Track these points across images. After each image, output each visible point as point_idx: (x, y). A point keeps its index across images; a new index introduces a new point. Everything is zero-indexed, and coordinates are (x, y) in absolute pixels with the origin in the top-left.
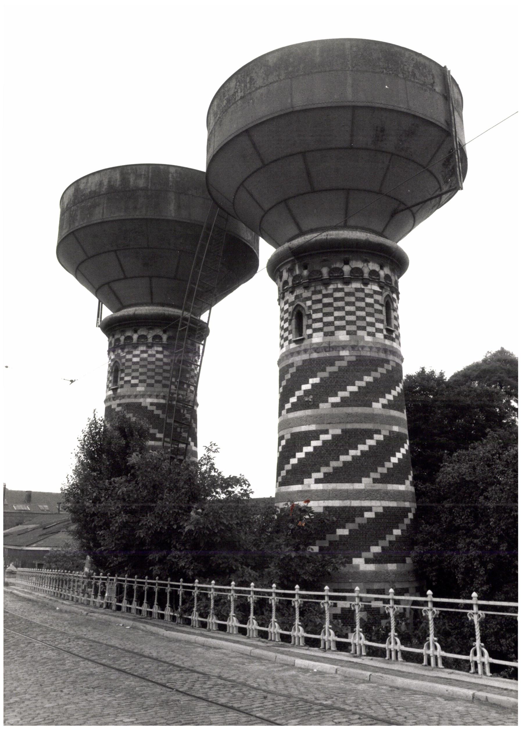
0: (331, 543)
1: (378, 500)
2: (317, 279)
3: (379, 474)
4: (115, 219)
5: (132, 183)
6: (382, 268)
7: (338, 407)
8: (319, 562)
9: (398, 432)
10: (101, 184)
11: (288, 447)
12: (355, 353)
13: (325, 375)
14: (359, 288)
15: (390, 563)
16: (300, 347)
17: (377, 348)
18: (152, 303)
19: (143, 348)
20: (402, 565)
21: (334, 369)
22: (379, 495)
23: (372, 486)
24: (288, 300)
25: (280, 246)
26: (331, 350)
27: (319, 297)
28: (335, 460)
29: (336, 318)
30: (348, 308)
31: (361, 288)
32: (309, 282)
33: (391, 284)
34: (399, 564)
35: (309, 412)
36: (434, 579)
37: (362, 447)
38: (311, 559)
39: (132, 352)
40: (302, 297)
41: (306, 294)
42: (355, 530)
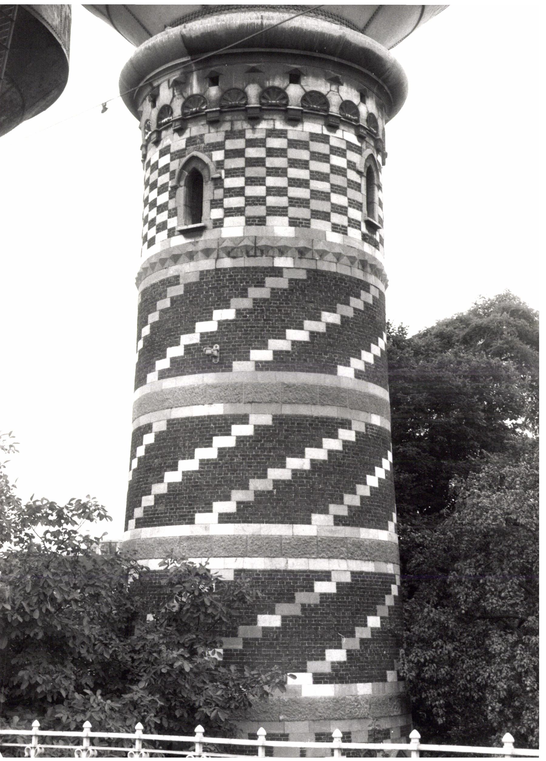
0: (247, 642)
1: (342, 558)
2: (236, 106)
3: (346, 508)
6: (363, 100)
7: (267, 370)
8: (233, 680)
9: (380, 428)
11: (160, 448)
12: (306, 264)
13: (246, 303)
14: (317, 134)
15: (361, 682)
16: (194, 244)
17: (350, 257)
20: (381, 684)
21: (263, 293)
22: (344, 549)
23: (331, 531)
24: (169, 146)
26: (259, 253)
27: (239, 144)
28: (259, 478)
29: (271, 191)
30: (293, 173)
31: (322, 135)
32: (220, 111)
33: (357, 121)
34: (376, 684)
35: (209, 378)
36: (441, 712)
37: (314, 454)
38: (211, 674)
40: (203, 142)
41: (213, 136)
42: (294, 617)
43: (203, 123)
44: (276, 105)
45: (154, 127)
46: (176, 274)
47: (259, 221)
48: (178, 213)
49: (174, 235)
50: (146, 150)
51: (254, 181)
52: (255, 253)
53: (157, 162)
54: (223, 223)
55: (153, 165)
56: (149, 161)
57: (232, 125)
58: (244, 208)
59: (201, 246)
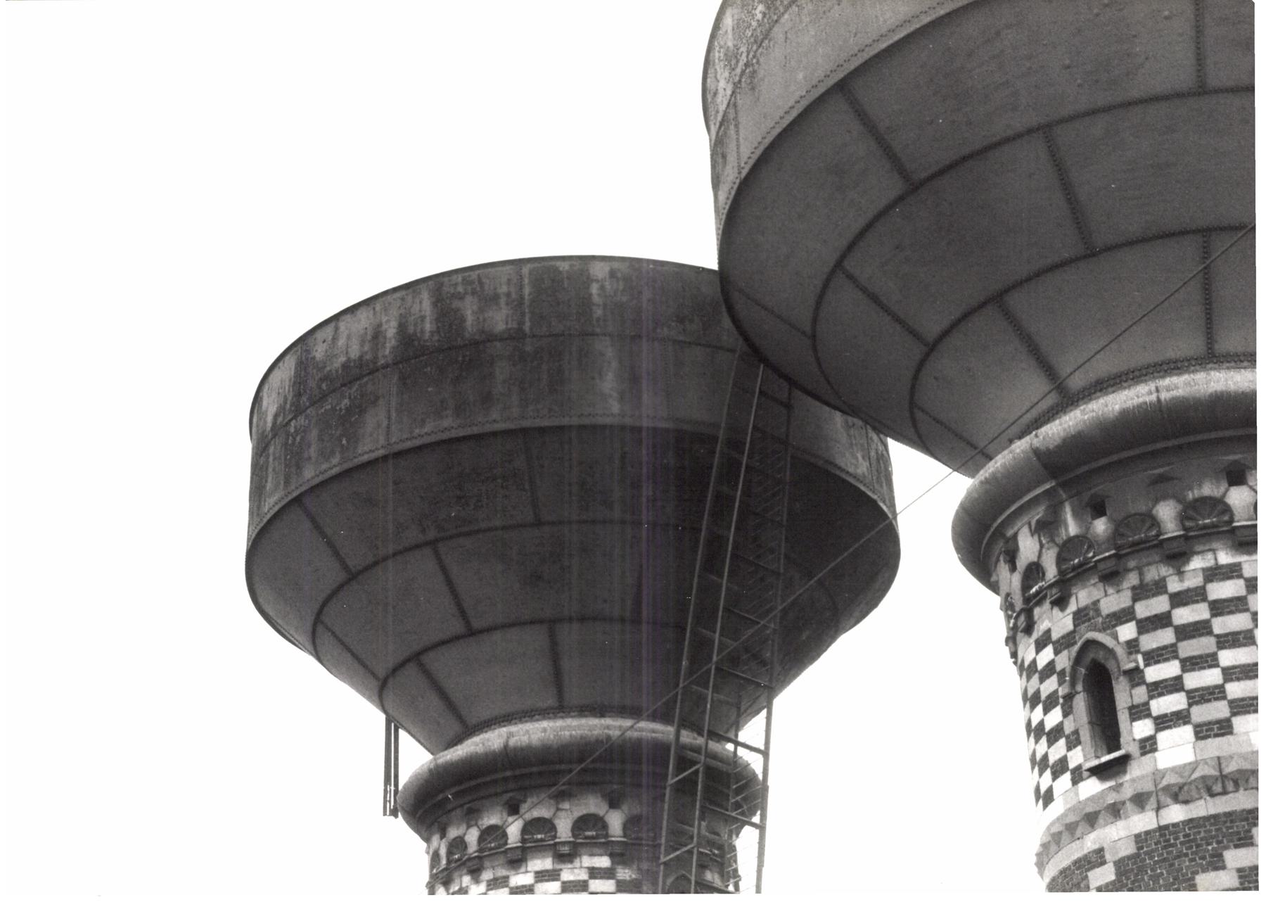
4: (427, 440)
5: (470, 319)
10: (377, 335)
18: (560, 709)
19: (545, 863)
24: (1048, 631)
25: (991, 459)
26: (1230, 786)
27: (1159, 605)
32: (1117, 556)
39: (506, 878)
40: (1098, 612)
41: (1113, 601)
43: (1092, 582)
44: (1214, 526)
45: (1019, 605)
46: (1096, 847)
47: (1219, 729)
48: (1082, 739)
49: (1082, 779)
50: (1015, 644)
51: (1197, 664)
52: (1224, 787)
53: (1034, 661)
54: (1155, 743)
55: (1029, 666)
56: (1023, 661)
57: (1141, 574)
58: (1188, 710)
59: (1128, 792)
